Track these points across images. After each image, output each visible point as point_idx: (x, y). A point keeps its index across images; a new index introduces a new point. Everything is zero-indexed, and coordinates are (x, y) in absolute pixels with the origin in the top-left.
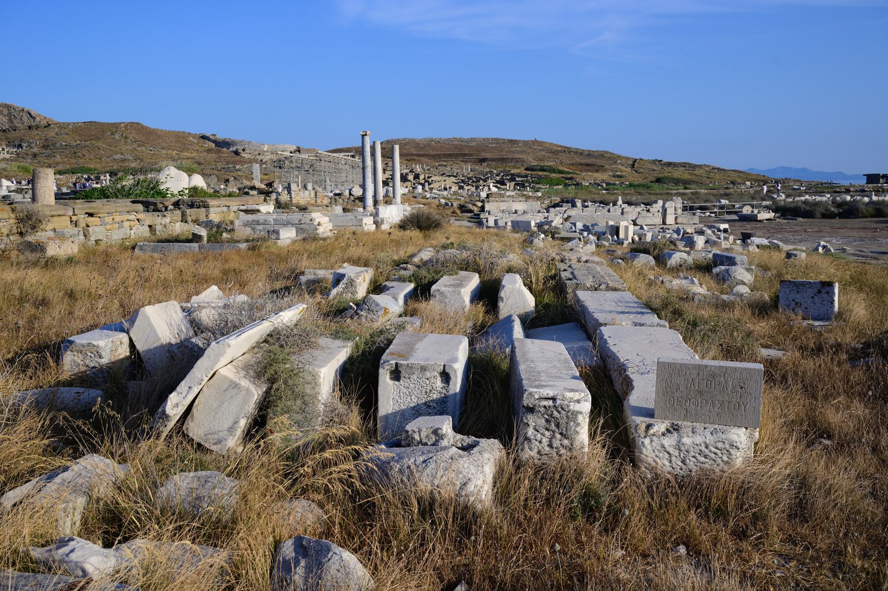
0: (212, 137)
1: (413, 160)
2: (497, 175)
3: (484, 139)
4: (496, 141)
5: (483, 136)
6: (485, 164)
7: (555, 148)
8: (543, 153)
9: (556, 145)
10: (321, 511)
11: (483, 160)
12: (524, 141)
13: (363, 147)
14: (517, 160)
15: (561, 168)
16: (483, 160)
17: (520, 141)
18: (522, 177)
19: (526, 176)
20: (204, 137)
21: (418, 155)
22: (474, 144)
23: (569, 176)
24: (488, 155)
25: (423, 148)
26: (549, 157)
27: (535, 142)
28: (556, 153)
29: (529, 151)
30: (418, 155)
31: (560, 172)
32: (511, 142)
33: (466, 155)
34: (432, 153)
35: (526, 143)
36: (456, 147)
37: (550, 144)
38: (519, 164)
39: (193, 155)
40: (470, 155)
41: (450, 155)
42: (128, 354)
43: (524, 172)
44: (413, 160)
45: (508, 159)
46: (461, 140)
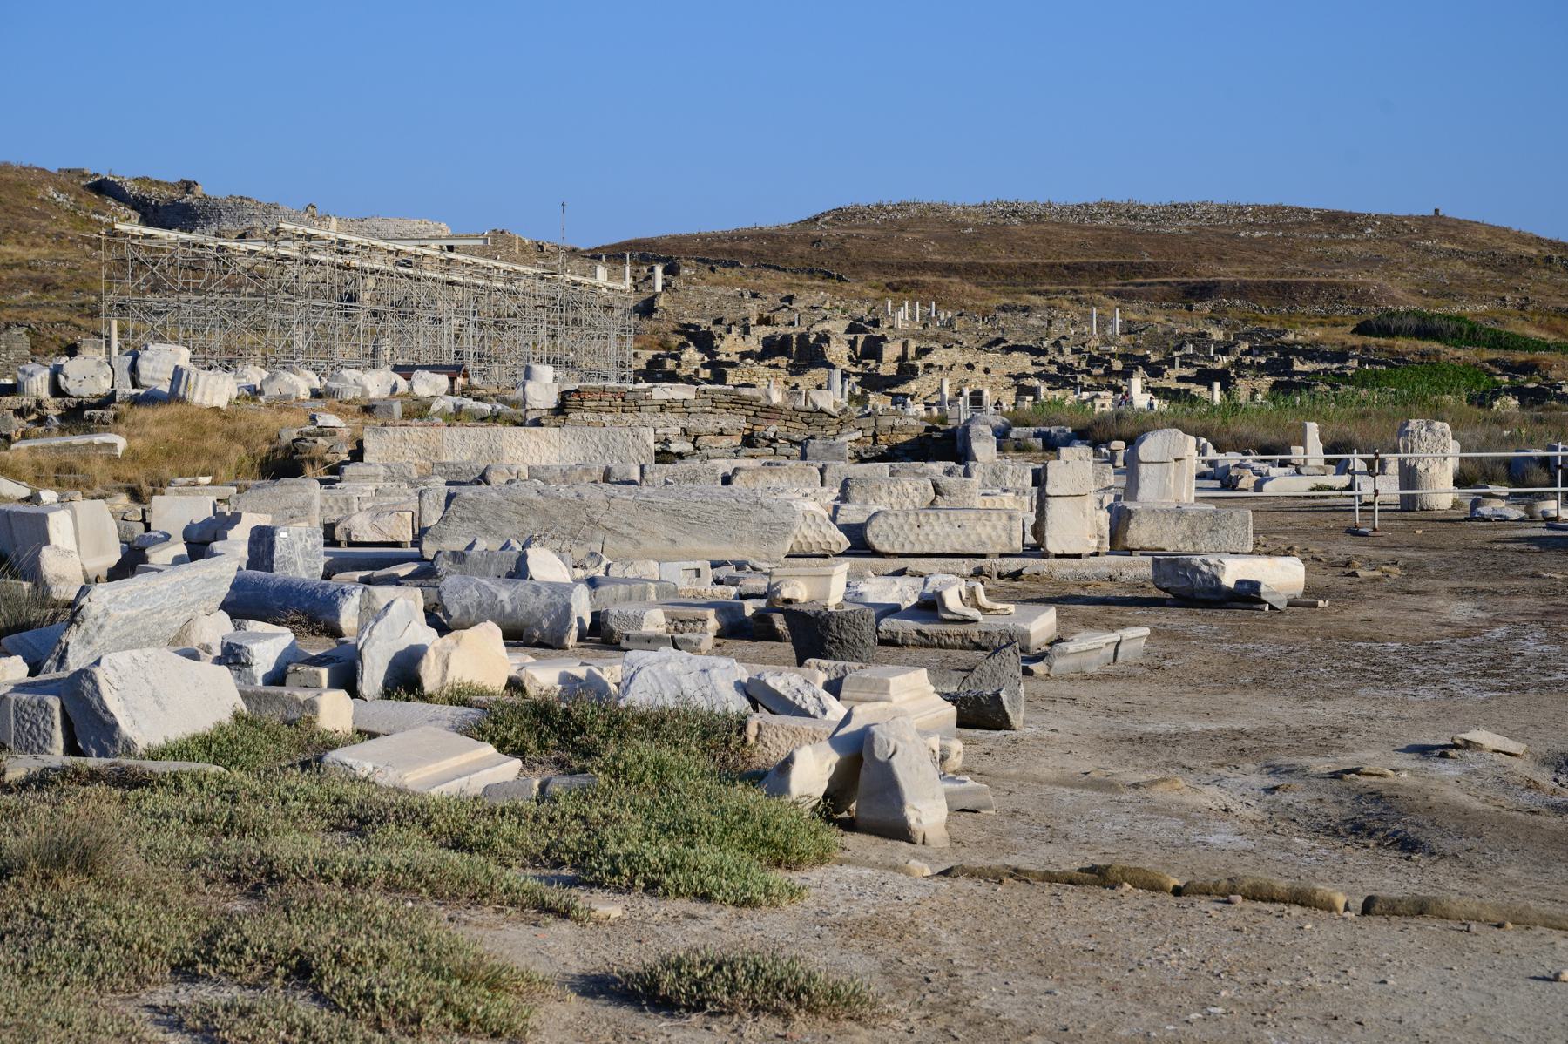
0: (131, 188)
1: (915, 285)
2: (1224, 351)
3: (1223, 210)
4: (1274, 216)
5: (1221, 199)
6: (1206, 307)
7: (1514, 248)
8: (1460, 266)
9: (1521, 238)
10: (700, 658)
11: (1204, 291)
12: (1386, 219)
13: (1046, 555)
14: (1338, 294)
15: (1516, 327)
16: (1204, 291)
17: (1368, 219)
18: (1323, 357)
19: (1341, 356)
20: (104, 188)
21: (949, 269)
22: (1182, 226)
23: (1521, 357)
24: (1227, 273)
25: (972, 241)
26: (1481, 284)
27: (1435, 223)
28: (1513, 266)
29: (1404, 255)
30: (949, 269)
31: (1498, 341)
32: (1336, 221)
33: (1137, 269)
34: (1003, 258)
35: (1393, 227)
36: (1105, 239)
37: (1494, 231)
38: (1344, 311)
39: (32, 254)
40: (1155, 269)
41: (1075, 270)
42: (141, 746)
43: (1342, 336)
44: (915, 285)
45: (1300, 286)
46: (1132, 212)
